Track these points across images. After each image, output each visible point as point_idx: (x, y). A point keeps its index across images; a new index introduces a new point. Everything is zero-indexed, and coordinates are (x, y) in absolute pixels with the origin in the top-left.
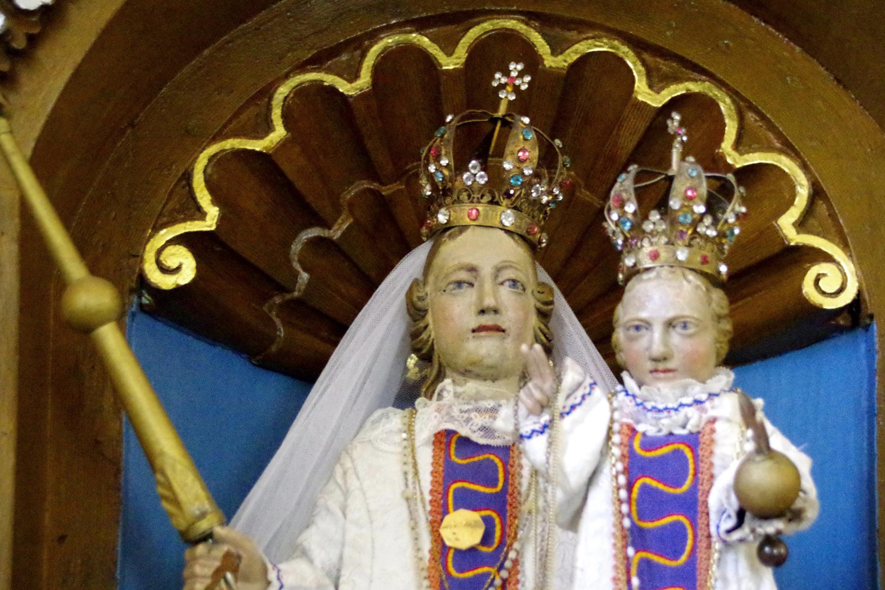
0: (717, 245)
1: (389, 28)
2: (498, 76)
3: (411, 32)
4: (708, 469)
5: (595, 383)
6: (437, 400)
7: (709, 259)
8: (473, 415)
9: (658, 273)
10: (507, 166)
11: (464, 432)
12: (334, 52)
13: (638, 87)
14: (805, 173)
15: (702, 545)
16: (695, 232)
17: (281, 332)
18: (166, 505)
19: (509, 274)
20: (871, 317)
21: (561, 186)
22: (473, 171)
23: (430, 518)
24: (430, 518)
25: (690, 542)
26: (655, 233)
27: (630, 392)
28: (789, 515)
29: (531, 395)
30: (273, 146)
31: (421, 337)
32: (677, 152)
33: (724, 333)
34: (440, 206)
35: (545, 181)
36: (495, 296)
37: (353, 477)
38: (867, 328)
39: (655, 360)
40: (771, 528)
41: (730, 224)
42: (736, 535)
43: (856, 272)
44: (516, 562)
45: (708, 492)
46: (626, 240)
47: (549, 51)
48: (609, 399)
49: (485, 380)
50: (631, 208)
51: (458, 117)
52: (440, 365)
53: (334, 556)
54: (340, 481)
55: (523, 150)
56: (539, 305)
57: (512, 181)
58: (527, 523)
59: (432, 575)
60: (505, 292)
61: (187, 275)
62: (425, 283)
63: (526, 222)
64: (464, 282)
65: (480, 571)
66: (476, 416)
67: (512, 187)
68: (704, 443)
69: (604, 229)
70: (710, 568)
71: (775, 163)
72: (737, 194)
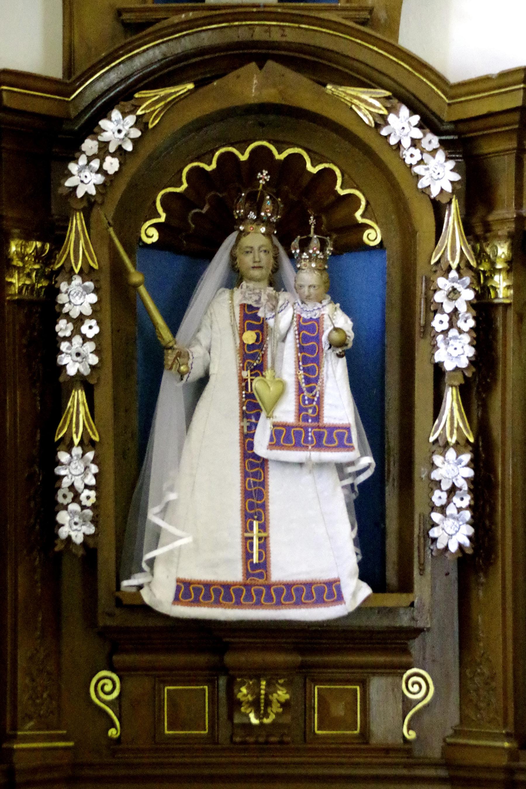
8: (252, 295)
15: (321, 351)
18: (159, 339)
19: (263, 248)
60: (262, 255)
61: (155, 238)
65: (255, 351)
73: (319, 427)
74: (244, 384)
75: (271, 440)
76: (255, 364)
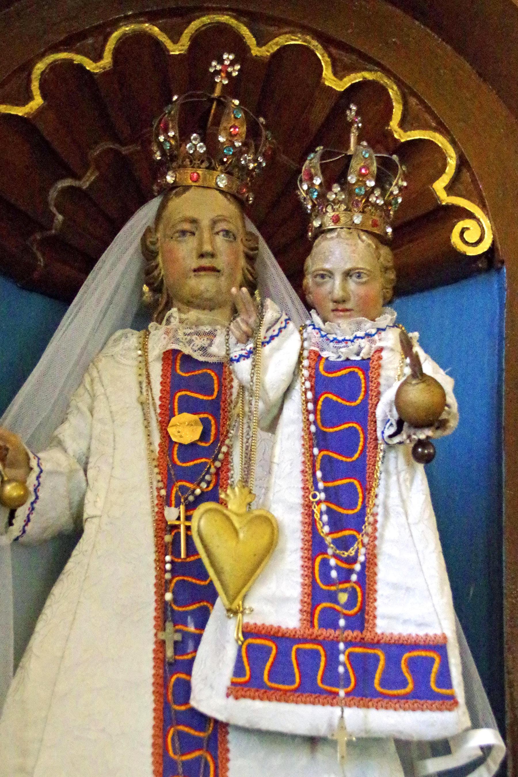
0: (385, 212)
1: (127, 19)
2: (214, 63)
3: (145, 22)
4: (376, 388)
5: (289, 319)
6: (166, 325)
7: (379, 223)
8: (194, 337)
9: (338, 233)
10: (221, 139)
11: (187, 351)
12: (82, 35)
13: (325, 74)
14: (454, 148)
16: (367, 201)
17: (41, 262)
20: (503, 262)
21: (264, 156)
22: (194, 142)
23: (160, 419)
24: (160, 419)
25: (361, 444)
26: (337, 201)
27: (317, 327)
28: (436, 424)
29: (239, 327)
30: (32, 112)
31: (153, 274)
32: (355, 136)
33: (390, 281)
34: (168, 169)
35: (253, 150)
36: (212, 242)
37: (99, 385)
38: (499, 270)
39: (336, 302)
40: (422, 435)
41: (395, 195)
42: (396, 440)
43: (492, 227)
44: (227, 454)
45: (376, 405)
46: (314, 206)
47: (255, 42)
48: (300, 331)
49: (204, 309)
50: (317, 181)
51: (183, 96)
52: (168, 295)
53: (83, 445)
54: (88, 387)
55: (235, 127)
56: (246, 250)
57: (225, 151)
58: (236, 424)
59: (161, 464)
60: (220, 240)
62: (156, 230)
63: (236, 185)
64: (188, 232)
66: (196, 339)
67: (226, 156)
68: (373, 368)
69: (297, 195)
70: (376, 464)
71: (431, 139)
72: (400, 172)
73: (362, 643)
74: (168, 538)
75: (239, 670)
76: (198, 491)
